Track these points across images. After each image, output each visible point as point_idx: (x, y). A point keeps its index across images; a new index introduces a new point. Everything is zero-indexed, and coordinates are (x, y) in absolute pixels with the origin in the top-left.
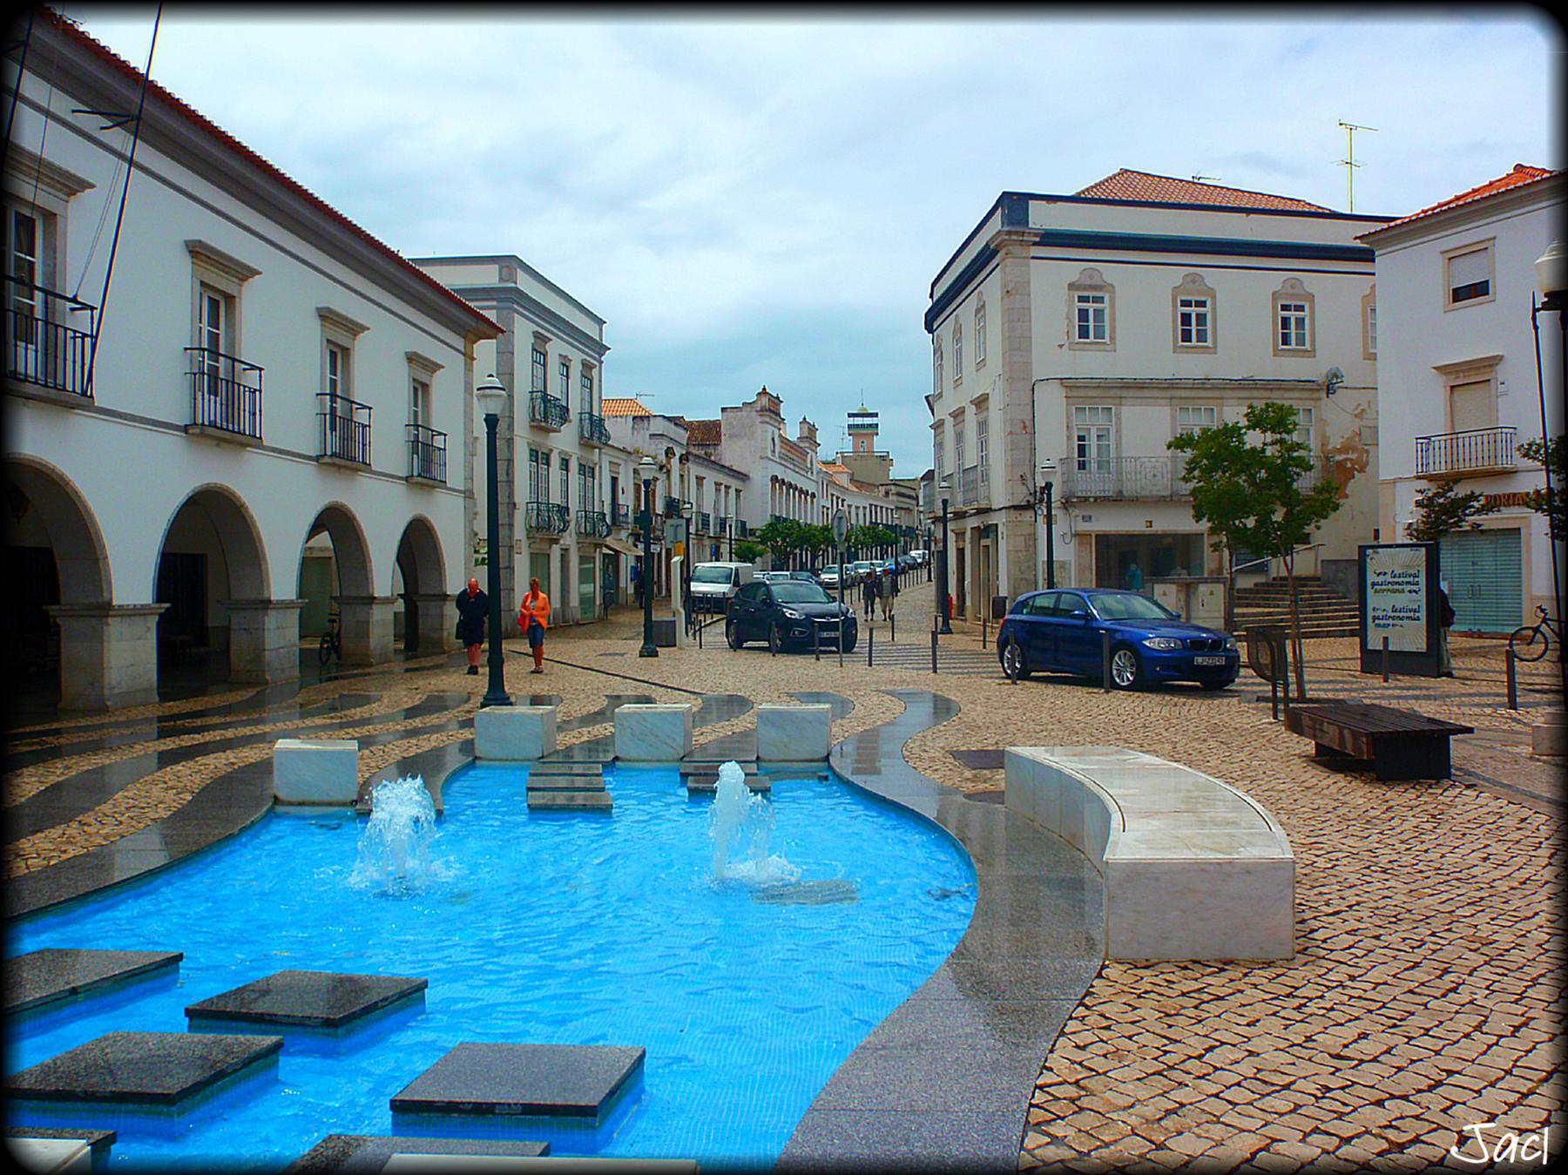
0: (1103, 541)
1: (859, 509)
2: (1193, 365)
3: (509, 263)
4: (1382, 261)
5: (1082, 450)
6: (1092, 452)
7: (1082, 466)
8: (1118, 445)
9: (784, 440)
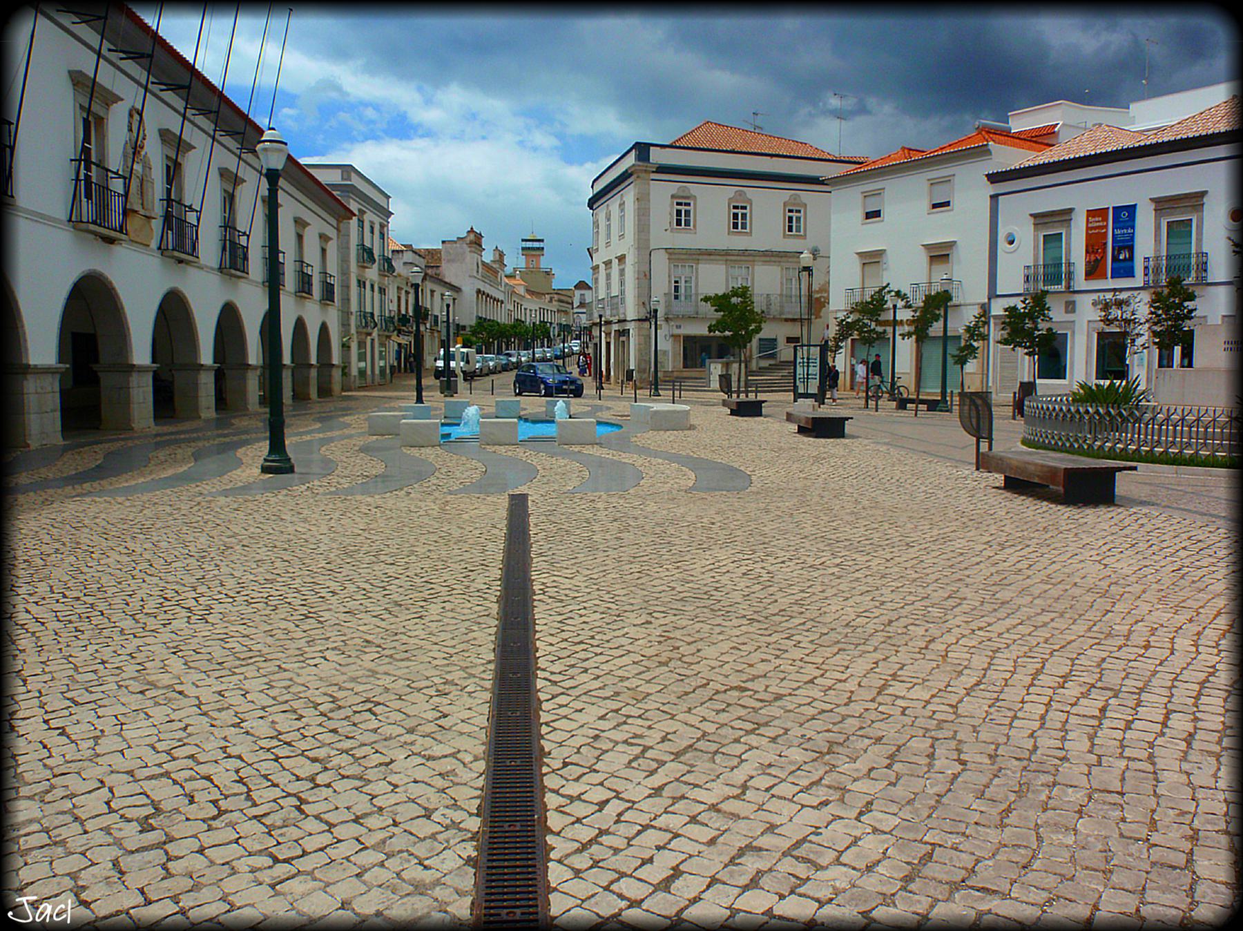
0: (688, 339)
1: (532, 311)
2: (739, 242)
3: (348, 169)
5: (676, 289)
6: (682, 290)
9: (484, 263)
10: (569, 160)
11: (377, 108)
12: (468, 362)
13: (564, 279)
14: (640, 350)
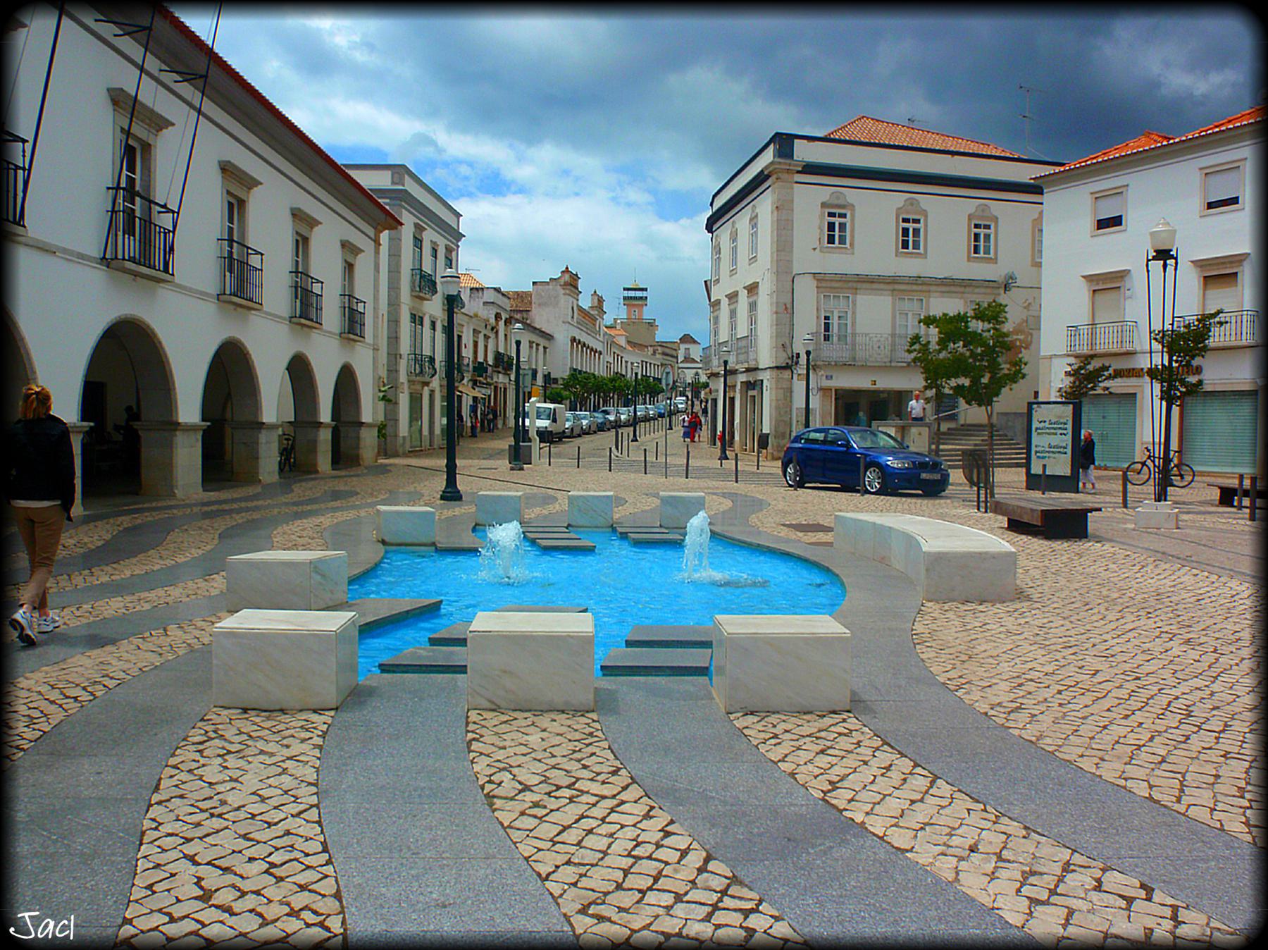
1: (633, 364)
2: (909, 266)
4: (1047, 198)
6: (835, 329)
7: (827, 338)
8: (854, 324)
10: (663, 216)
11: (471, 165)
12: (554, 421)
13: (667, 333)
14: (777, 408)
